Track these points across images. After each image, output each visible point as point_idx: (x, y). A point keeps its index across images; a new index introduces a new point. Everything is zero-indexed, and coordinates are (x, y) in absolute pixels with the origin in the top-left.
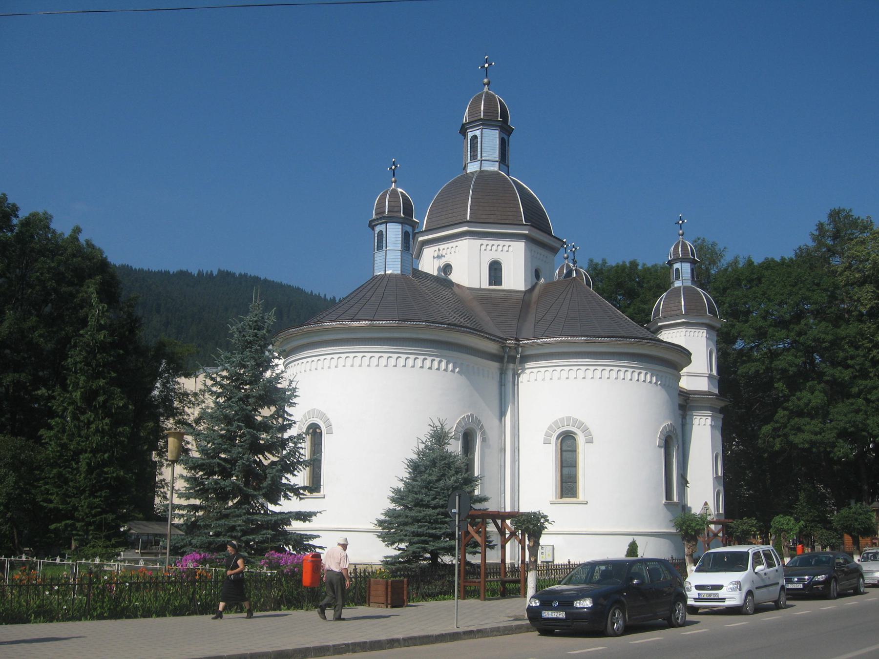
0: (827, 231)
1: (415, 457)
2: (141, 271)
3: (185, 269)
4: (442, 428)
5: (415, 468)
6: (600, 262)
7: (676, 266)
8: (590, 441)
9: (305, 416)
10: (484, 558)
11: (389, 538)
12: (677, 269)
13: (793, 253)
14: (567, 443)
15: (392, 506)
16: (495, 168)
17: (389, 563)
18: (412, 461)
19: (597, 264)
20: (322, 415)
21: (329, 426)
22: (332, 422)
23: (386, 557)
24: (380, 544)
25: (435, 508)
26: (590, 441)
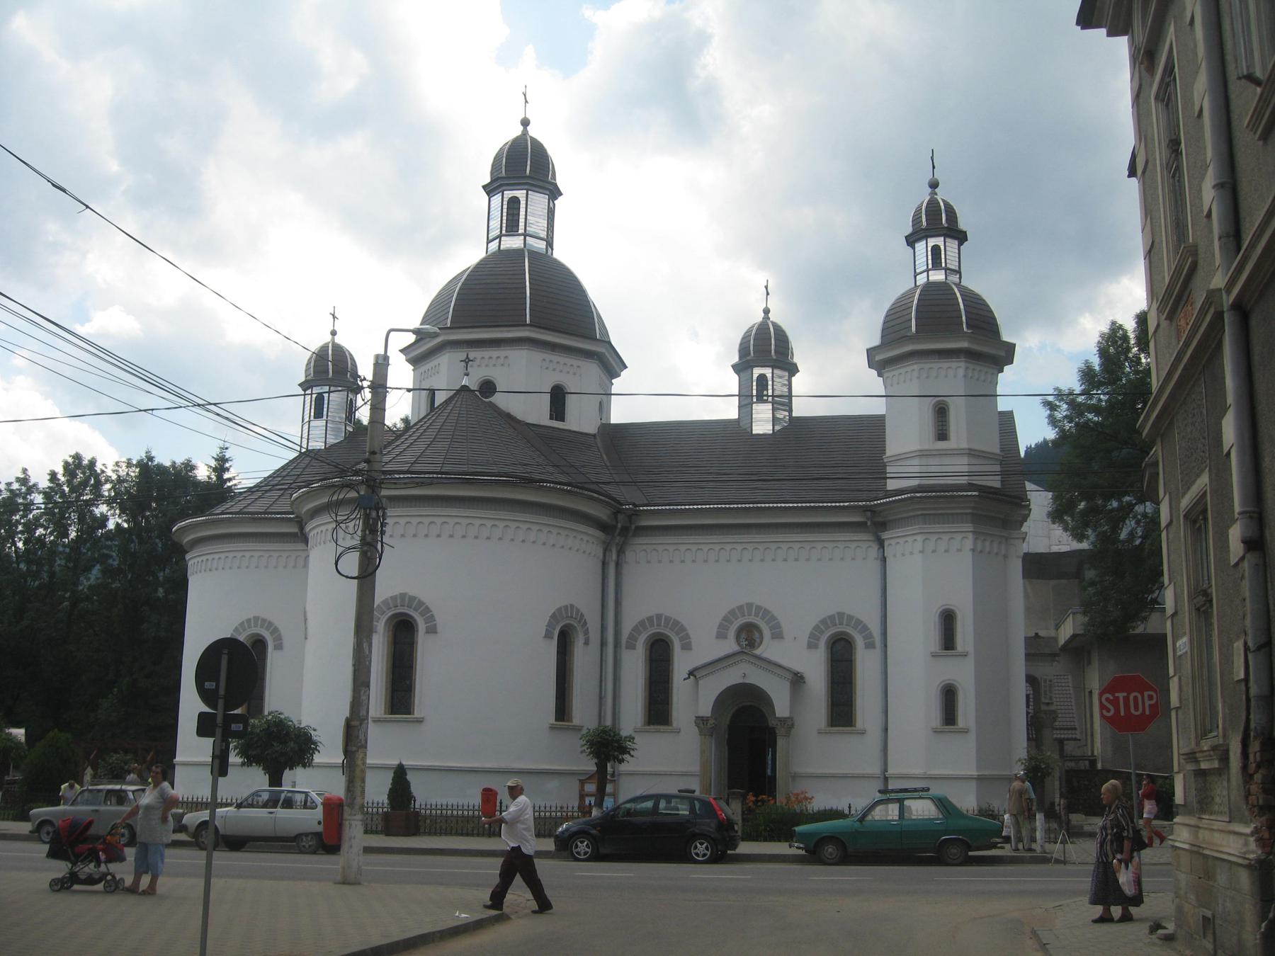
3: (1041, 440)
8: (432, 630)
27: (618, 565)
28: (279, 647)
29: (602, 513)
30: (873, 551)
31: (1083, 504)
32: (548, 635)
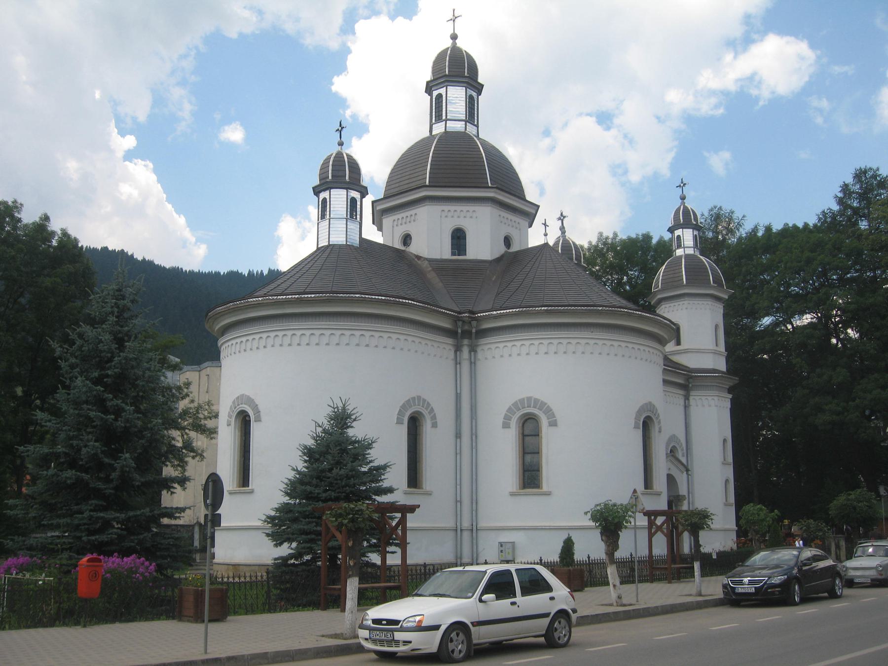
0: (853, 192)
1: (310, 442)
2: (192, 273)
3: (235, 270)
4: (344, 408)
5: (310, 454)
6: (611, 236)
7: (678, 232)
8: (553, 424)
9: (234, 402)
10: (384, 560)
11: (278, 538)
12: (679, 237)
13: (816, 218)
14: (529, 429)
15: (286, 499)
16: (459, 126)
17: (282, 563)
18: (305, 447)
19: (607, 238)
20: (250, 401)
21: (257, 412)
22: (261, 408)
23: (276, 559)
24: (269, 543)
25: (326, 500)
26: (553, 424)
27: (473, 364)
28: (258, 419)
29: (446, 324)
30: (448, 365)
31: (849, 331)
32: (399, 422)
